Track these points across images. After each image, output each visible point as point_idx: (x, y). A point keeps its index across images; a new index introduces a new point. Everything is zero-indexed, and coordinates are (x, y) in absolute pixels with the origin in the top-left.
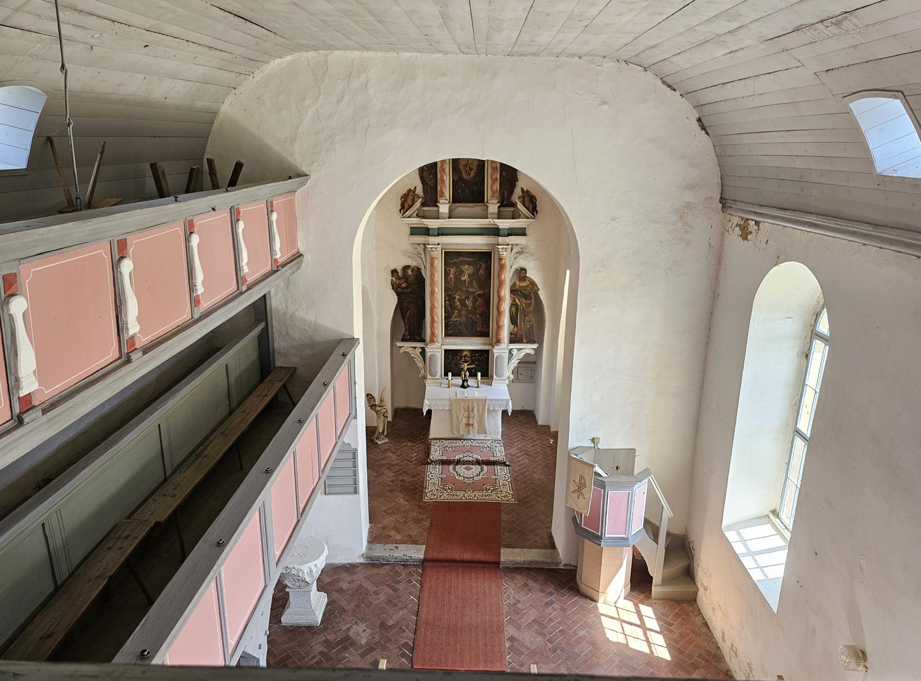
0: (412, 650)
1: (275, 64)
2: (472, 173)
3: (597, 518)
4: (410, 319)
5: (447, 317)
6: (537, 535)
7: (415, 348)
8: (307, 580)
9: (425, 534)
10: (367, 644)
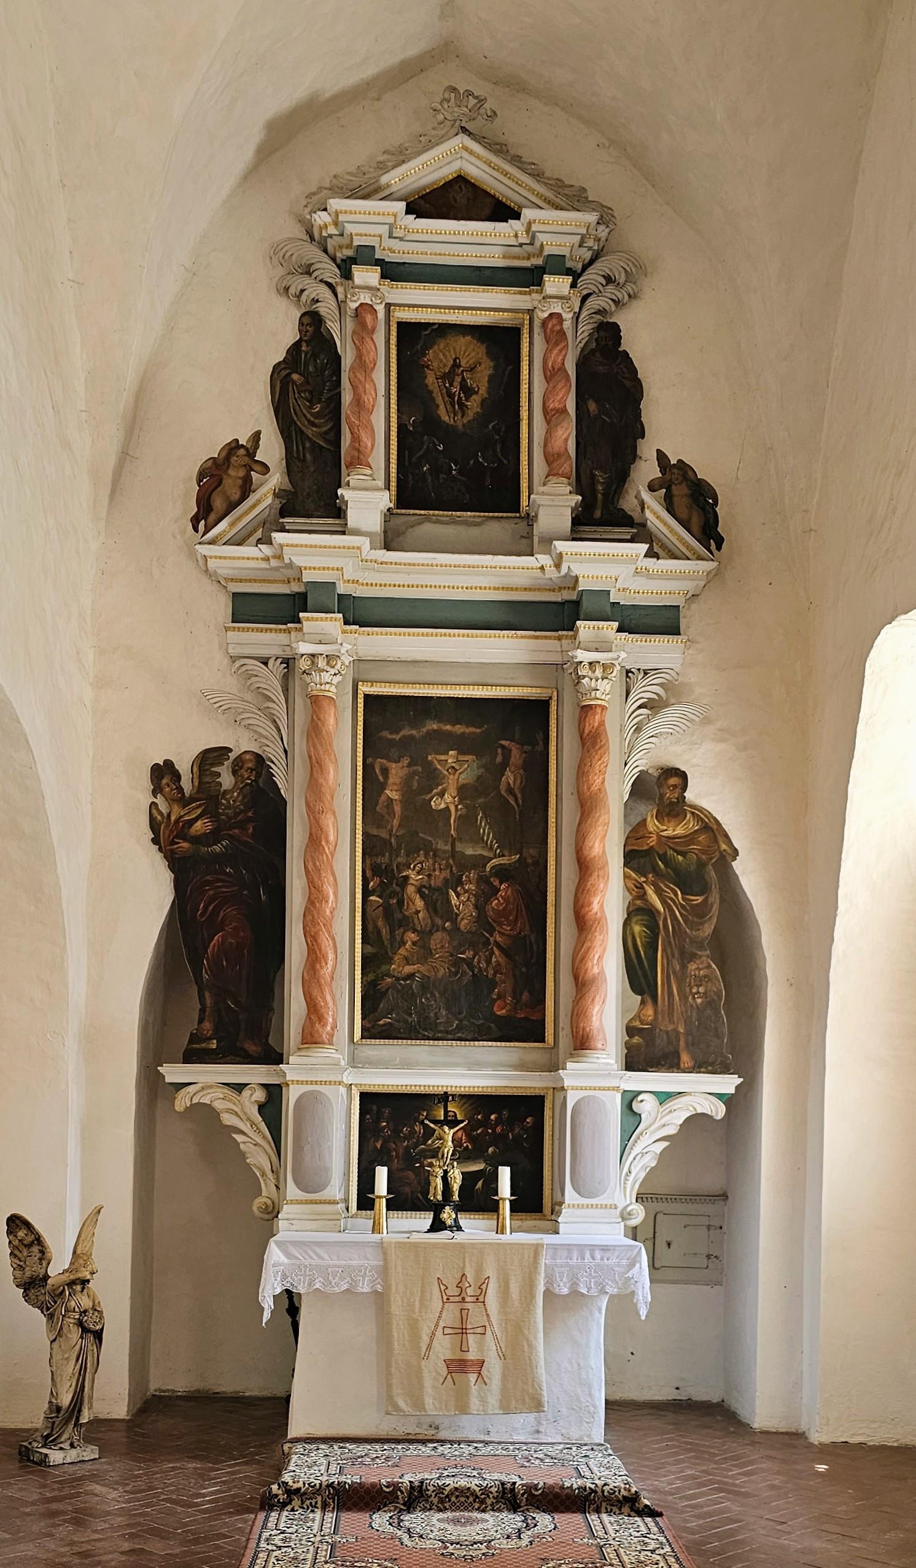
2: (474, 404)
4: (220, 978)
5: (374, 961)
7: (239, 1088)
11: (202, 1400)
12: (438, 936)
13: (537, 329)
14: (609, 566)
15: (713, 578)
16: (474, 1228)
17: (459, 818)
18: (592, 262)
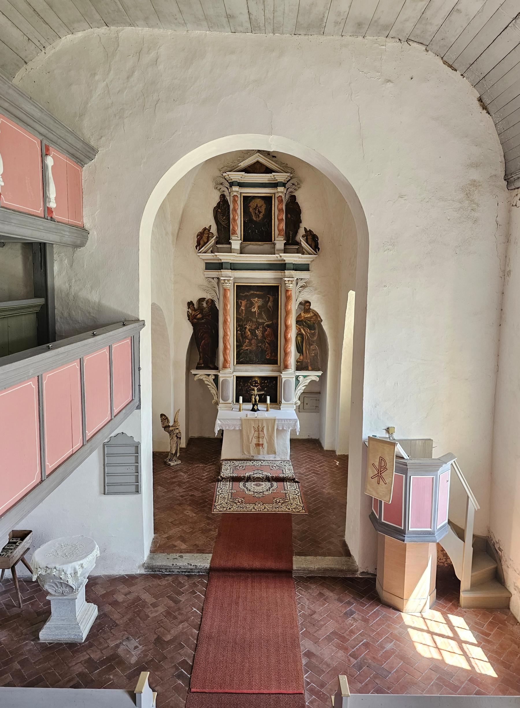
0: (191, 669)
1: (68, 40)
2: (261, 215)
3: (398, 508)
4: (204, 350)
6: (331, 543)
7: (209, 375)
8: (71, 583)
9: (213, 543)
10: (137, 663)
12: (253, 340)
13: (276, 198)
17: (258, 313)
18: (289, 180)
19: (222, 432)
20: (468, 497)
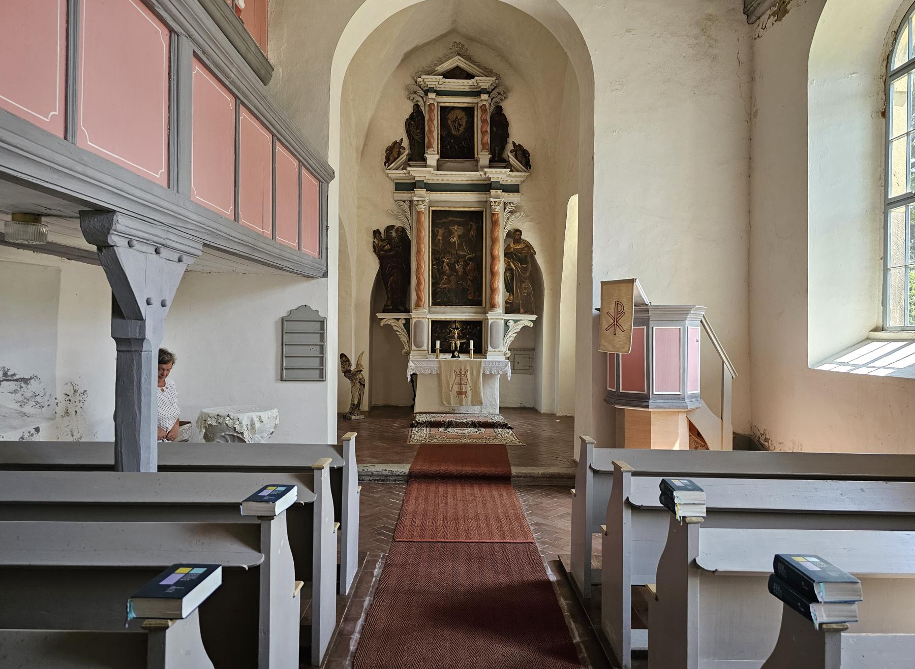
3: (639, 367)
4: (392, 290)
7: (398, 319)
11: (386, 407)
14: (499, 175)
15: (527, 176)
16: (463, 357)
19: (414, 375)
20: (723, 362)
